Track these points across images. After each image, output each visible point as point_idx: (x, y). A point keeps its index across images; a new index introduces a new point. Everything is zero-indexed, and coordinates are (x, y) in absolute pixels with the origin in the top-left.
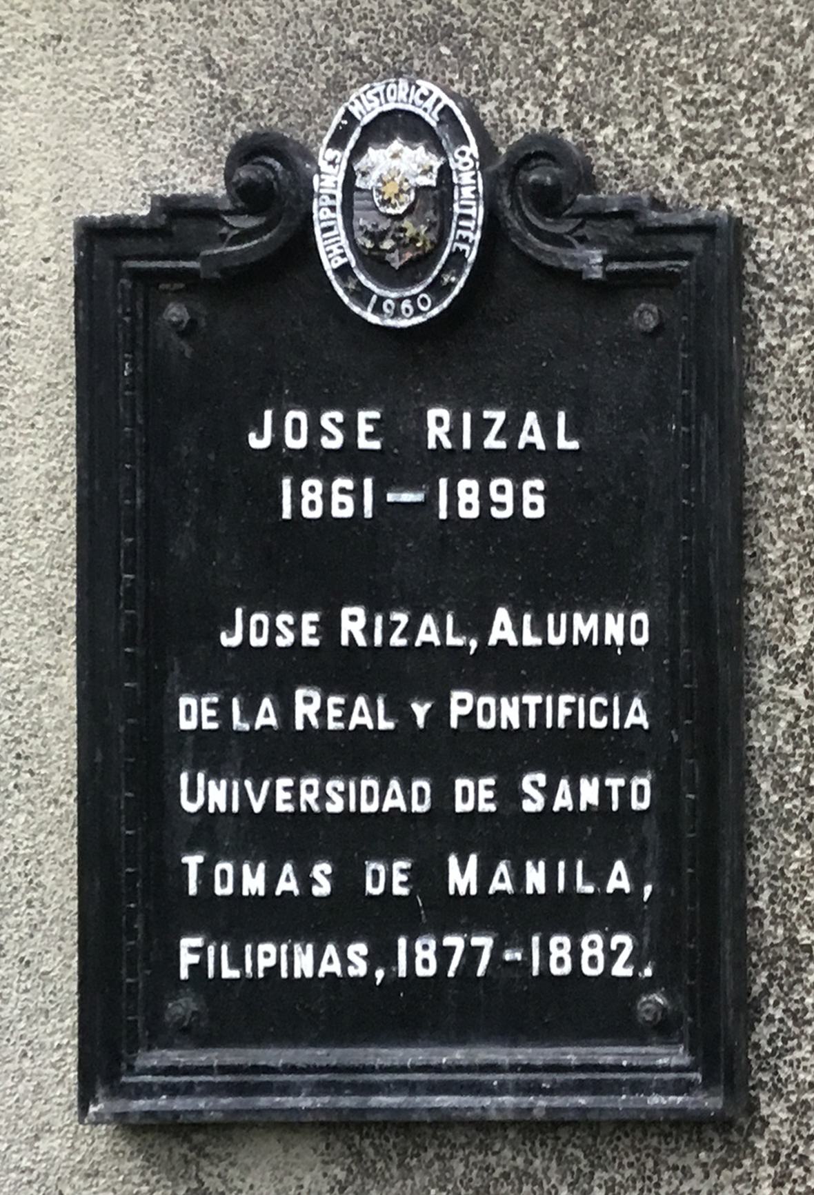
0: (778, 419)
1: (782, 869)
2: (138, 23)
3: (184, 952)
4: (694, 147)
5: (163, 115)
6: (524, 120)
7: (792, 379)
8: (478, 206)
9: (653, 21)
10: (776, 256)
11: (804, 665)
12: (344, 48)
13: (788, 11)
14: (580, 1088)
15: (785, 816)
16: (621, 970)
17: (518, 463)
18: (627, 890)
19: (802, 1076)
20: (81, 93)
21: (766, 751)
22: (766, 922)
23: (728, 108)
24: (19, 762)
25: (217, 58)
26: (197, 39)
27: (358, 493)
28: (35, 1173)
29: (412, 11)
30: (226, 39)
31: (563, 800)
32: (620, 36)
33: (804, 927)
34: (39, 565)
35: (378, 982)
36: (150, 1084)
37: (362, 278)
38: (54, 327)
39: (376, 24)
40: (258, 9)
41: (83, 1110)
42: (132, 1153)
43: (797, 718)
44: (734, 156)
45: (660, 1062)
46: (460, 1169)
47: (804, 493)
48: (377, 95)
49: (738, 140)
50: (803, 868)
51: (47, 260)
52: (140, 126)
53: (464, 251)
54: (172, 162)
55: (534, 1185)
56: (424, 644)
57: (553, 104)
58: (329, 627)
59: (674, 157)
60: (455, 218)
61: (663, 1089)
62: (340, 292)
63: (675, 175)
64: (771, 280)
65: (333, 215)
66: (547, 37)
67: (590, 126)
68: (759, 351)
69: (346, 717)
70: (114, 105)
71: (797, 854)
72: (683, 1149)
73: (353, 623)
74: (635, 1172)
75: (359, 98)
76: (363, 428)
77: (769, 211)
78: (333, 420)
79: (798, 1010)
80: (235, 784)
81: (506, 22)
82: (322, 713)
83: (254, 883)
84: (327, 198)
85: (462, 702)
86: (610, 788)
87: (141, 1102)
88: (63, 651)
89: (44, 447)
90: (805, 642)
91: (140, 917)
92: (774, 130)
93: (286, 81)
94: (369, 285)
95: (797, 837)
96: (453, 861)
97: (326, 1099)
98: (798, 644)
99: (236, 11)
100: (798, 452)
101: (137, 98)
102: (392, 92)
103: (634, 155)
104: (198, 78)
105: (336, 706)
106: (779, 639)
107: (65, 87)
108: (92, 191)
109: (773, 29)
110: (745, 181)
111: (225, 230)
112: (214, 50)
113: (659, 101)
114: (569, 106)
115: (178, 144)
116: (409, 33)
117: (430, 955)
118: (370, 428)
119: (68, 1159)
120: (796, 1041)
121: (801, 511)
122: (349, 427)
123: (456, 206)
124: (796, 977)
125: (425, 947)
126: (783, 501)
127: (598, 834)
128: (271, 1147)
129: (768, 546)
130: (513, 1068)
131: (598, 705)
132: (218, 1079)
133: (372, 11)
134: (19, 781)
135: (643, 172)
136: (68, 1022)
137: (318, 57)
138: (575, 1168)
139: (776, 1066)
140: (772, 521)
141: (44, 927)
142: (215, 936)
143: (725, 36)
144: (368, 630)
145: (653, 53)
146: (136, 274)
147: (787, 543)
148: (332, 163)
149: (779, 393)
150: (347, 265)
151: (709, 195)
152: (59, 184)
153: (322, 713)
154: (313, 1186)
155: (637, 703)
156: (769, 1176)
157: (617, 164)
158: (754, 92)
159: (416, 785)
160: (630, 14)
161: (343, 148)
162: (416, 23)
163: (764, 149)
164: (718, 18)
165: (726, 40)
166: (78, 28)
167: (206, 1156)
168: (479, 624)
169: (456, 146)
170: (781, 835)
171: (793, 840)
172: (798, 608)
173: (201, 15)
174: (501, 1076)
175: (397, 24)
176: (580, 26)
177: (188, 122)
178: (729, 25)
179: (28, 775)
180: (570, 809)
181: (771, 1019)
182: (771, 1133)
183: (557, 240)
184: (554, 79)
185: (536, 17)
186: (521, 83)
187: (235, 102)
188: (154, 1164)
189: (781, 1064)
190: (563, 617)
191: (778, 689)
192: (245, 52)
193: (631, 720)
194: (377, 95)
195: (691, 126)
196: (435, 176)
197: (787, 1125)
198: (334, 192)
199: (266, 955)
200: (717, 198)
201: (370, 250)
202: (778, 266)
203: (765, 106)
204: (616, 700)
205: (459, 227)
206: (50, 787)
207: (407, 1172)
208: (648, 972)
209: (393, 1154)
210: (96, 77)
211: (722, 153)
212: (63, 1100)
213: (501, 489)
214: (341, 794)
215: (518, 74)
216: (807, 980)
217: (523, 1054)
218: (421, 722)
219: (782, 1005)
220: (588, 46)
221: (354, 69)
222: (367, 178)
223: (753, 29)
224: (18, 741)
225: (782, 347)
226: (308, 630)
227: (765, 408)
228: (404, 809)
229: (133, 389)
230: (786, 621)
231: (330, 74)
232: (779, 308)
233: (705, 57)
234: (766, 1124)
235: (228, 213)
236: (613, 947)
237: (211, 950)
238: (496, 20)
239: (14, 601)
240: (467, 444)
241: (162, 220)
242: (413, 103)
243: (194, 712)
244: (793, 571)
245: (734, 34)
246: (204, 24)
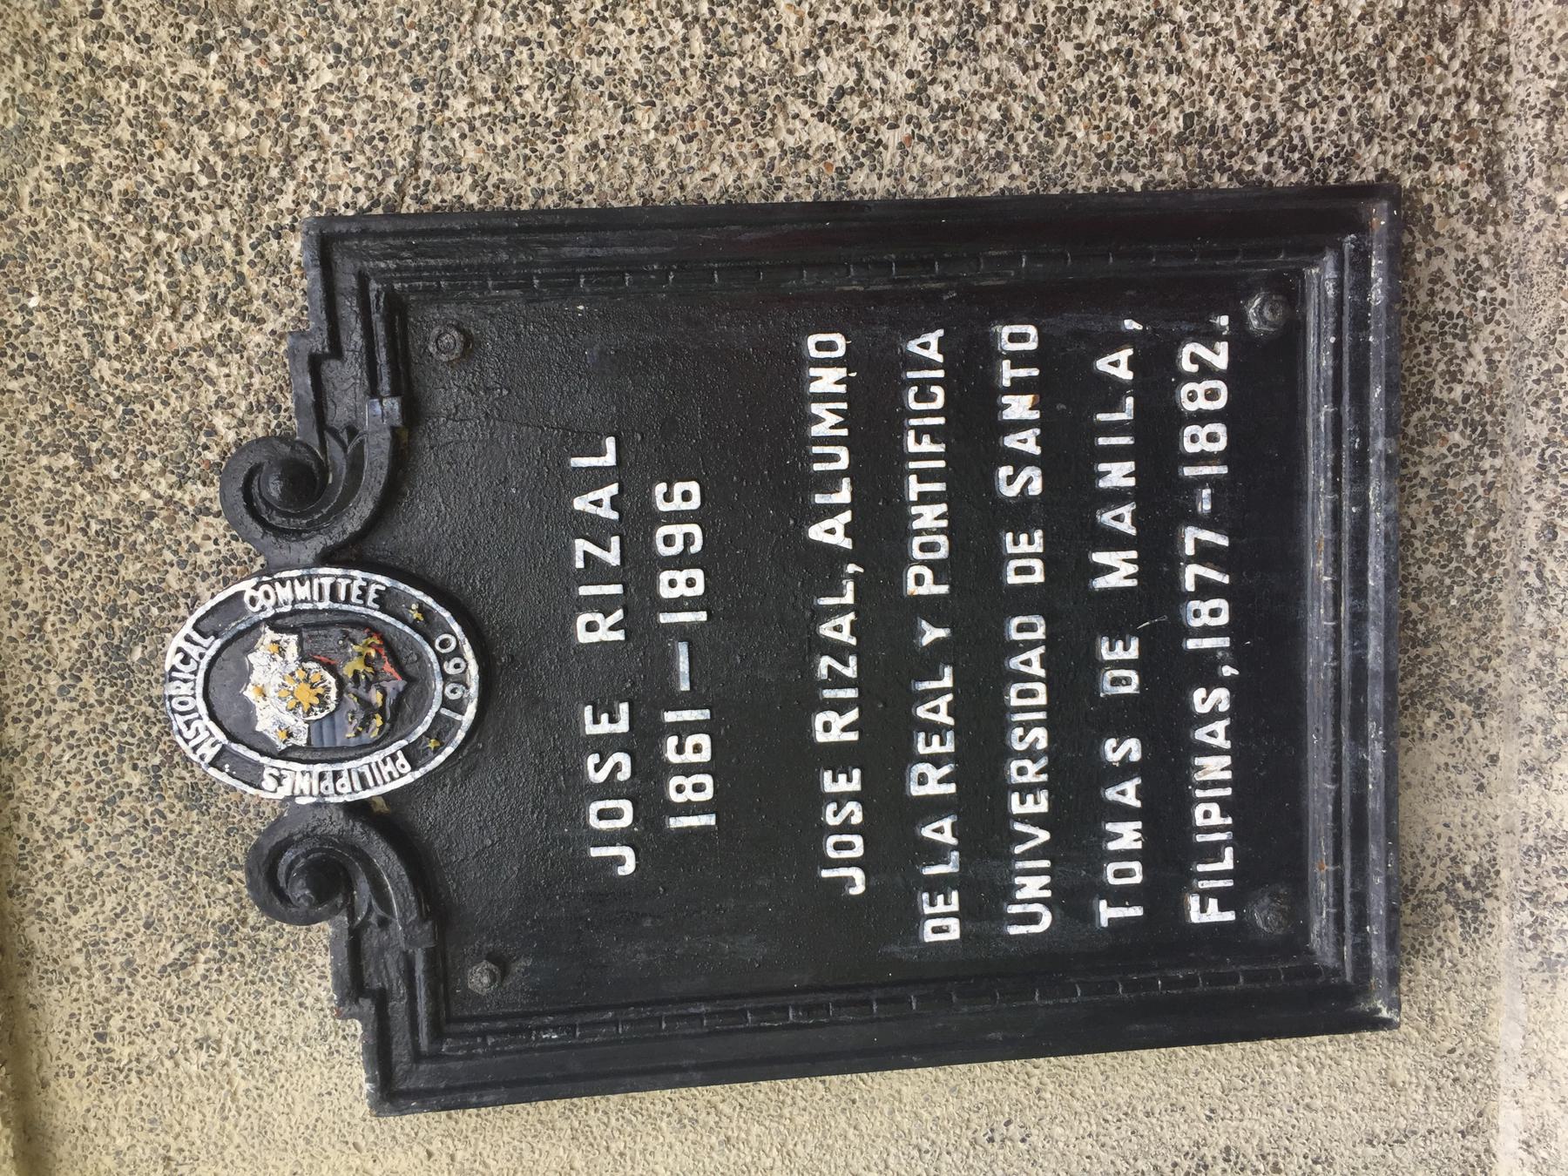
0: (562, 173)
1: (1098, 156)
2: (138, 1060)
3: (1205, 919)
4: (231, 302)
5: (246, 1020)
6: (216, 543)
7: (513, 154)
8: (319, 576)
9: (74, 366)
10: (360, 180)
11: (859, 131)
12: (146, 789)
13: (47, 174)
14: (1360, 399)
15: (1036, 153)
16: (1220, 358)
17: (637, 520)
18: (1130, 352)
19: (1332, 126)
20: (229, 1127)
21: (962, 181)
22: (1159, 176)
23: (177, 256)
24: (998, 1138)
25: (173, 955)
26: (151, 984)
28: (1430, 1083)
29: (92, 701)
30: (148, 946)
31: (1027, 442)
32: (98, 412)
33: (1164, 125)
34: (779, 1132)
35: (1236, 672)
36: (1354, 946)
37: (421, 730)
38: (506, 1138)
39: (112, 749)
40: (108, 906)
41: (1387, 1024)
42: (1411, 971)
43: (921, 139)
44: (237, 242)
45: (1330, 293)
46: (1430, 570)
47: (652, 134)
48: (188, 724)
49: (218, 240)
50: (1097, 127)
51: (430, 1155)
52: (262, 1049)
53: (377, 591)
54: (301, 1004)
55: (1447, 475)
56: (853, 633)
57: (192, 502)
58: (839, 758)
59: (246, 331)
60: (336, 606)
61: (1363, 285)
62: (441, 758)
63: (268, 327)
64: (390, 187)
65: (345, 774)
66: (108, 514)
67: (216, 450)
68: (480, 202)
69: (938, 729)
70: (241, 1085)
71: (1080, 135)
72: (1411, 281)
73: (833, 728)
74: (1436, 346)
75: (195, 749)
76: (605, 727)
77: (303, 191)
78: (597, 768)
79: (1259, 131)
80: (1019, 865)
81: (95, 571)
82: (937, 761)
83: (1128, 835)
84: (323, 785)
85: (919, 580)
86: (1013, 379)
87: (1374, 955)
88: (874, 1093)
89: (645, 1139)
90: (832, 130)
91: (1171, 974)
92: (200, 189)
93: (192, 864)
94: (429, 719)
95: (1061, 136)
96: (1100, 583)
97: (1371, 725)
98: (833, 140)
99: (113, 935)
100: (602, 144)
101: (228, 1056)
102: (182, 703)
103: (248, 387)
104: (198, 979)
105: (928, 743)
106: (829, 166)
107: (224, 1147)
108: (344, 1103)
109: (73, 195)
110: (268, 227)
111: (373, 919)
112: (163, 960)
113: (176, 353)
114: (194, 479)
115: (280, 999)
116: (120, 703)
117: (1205, 607)
118: (604, 717)
119: (1415, 1046)
120: (1294, 134)
121: (674, 139)
122: (605, 746)
123: (321, 606)
124: (1221, 135)
125: (1197, 614)
126: (663, 165)
127: (1067, 389)
128: (1406, 799)
129: (719, 183)
130: (1336, 487)
131: (918, 399)
132: (1348, 863)
133: (97, 755)
134: (1018, 1137)
135: (268, 372)
136: (1274, 1058)
137: (160, 824)
138: (1430, 423)
139: (1321, 160)
140: (688, 180)
141: (1173, 1095)
142: (1185, 881)
143: (86, 263)
144: (841, 707)
145: (116, 365)
146: (437, 1033)
147: (712, 159)
148: (279, 780)
149: (531, 173)
150: (404, 750)
151: (289, 279)
152: (338, 1146)
153: (937, 761)
154: (1445, 751)
155: (913, 346)
156: (1441, 168)
157: (260, 410)
158: (154, 219)
159: (1016, 636)
160: (70, 399)
161: (261, 767)
162: (106, 695)
163: (225, 204)
164: (64, 274)
165: (91, 260)
166: (152, 1136)
167: (1414, 881)
169: (245, 612)
170: (1059, 158)
171: (1064, 141)
172: (791, 142)
173: (121, 980)
174: (1346, 503)
175: (109, 720)
176: (91, 470)
177: (253, 988)
178: (72, 257)
179: (1012, 1127)
180: (1038, 431)
181: (1268, 169)
182: (1395, 166)
183: (356, 465)
184: (160, 503)
185: (84, 531)
186: (169, 548)
187: (224, 929)
188: (1422, 944)
189: (1318, 154)
190: (816, 450)
191: (888, 167)
192: (161, 920)
193: (933, 354)
194: (188, 724)
195: (203, 306)
196: (285, 637)
197: (1388, 145)
198: (315, 776)
199: (1208, 815)
200: (293, 267)
201: (384, 720)
202: (370, 176)
203: (170, 202)
204: (911, 375)
205: (347, 601)
206: (1022, 1098)
207: (1432, 637)
208: (1224, 321)
209: (1413, 653)
210: (208, 1110)
211: (235, 262)
212: (1356, 1057)
213: (669, 540)
214: (1026, 732)
215: (159, 553)
216: (1224, 119)
217: (1317, 481)
218: (942, 633)
219: (1253, 153)
220: (115, 456)
221: (170, 775)
222: (293, 730)
223: (74, 224)
224: (974, 1142)
225: (474, 169)
226: (843, 785)
227: (551, 193)
228: (1041, 650)
229: (574, 1027)
230: (807, 157)
231: (179, 806)
232: (425, 174)
233: (116, 290)
234: (1385, 171)
235: (352, 916)
236: (1194, 368)
237: (1205, 884)
238: (94, 586)
239: (820, 1160)
240: (616, 589)
241: (367, 1004)
242: (195, 673)
243: (941, 923)
244: (747, 148)
245: (83, 250)
246: (132, 975)
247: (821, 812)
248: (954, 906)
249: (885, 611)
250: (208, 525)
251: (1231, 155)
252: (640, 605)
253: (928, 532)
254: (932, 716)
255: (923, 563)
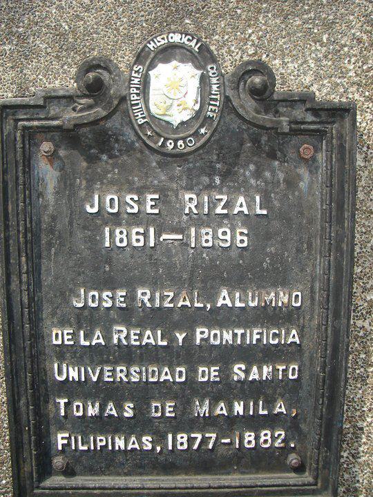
1: (353, 398)
27: (145, 235)
65: (138, 98)
81: (221, 9)
86: (237, 334)
118: (153, 203)
144: (152, 300)
153: (127, 338)
168: (211, 296)
219: (348, 451)
247: (108, 289)
248: (66, 343)
249: (190, 319)
250: (237, 53)
251: (348, 444)
252: (200, 221)
253: (222, 336)
254: (146, 336)
255: (209, 334)
